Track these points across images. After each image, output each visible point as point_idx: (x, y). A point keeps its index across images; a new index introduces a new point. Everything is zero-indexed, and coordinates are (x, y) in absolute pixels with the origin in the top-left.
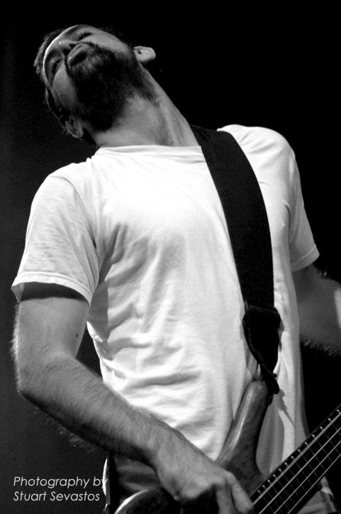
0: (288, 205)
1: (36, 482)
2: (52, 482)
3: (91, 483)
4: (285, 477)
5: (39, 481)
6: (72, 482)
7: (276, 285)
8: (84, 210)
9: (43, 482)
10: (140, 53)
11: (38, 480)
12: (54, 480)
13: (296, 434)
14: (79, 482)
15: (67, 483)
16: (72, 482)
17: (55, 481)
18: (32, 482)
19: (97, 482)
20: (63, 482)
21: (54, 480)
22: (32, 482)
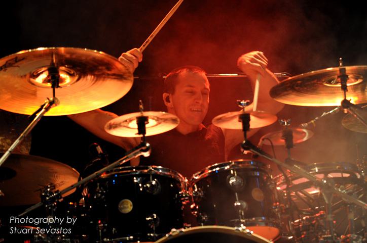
1: (26, 220)
2: (37, 221)
5: (28, 220)
6: (23, 221)
9: (31, 221)
11: (27, 218)
12: (39, 219)
14: (57, 220)
17: (40, 220)
18: (23, 221)
21: (39, 219)
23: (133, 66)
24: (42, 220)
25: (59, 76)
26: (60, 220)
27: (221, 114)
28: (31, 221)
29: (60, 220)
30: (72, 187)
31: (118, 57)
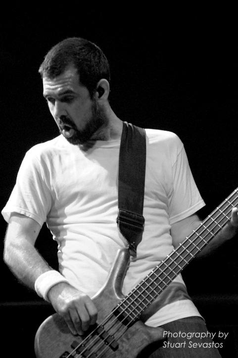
1: (178, 334)
2: (189, 335)
5: (181, 334)
6: (203, 335)
9: (175, 335)
11: (180, 333)
12: (191, 334)
14: (209, 335)
16: (203, 335)
17: (192, 334)
18: (175, 335)
21: (191, 334)
23: (72, 334)
24: (194, 334)
25: (198, 305)
26: (211, 335)
27: (41, 324)
28: (184, 335)
29: (211, 335)
30: (121, 252)
31: (185, 274)
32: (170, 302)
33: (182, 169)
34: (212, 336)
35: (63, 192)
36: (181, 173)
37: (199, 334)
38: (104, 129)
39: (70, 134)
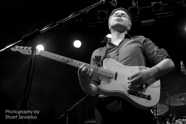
0: (97, 65)
1: (14, 112)
2: (19, 112)
3: (34, 112)
4: (133, 21)
5: (15, 112)
6: (26, 112)
7: (57, 55)
8: (158, 104)
9: (16, 112)
10: (101, 87)
11: (14, 111)
12: (24, 111)
13: (127, 41)
14: (29, 112)
15: (25, 112)
16: (26, 112)
17: (21, 112)
18: (12, 112)
19: (36, 112)
20: (23, 112)
21: (20, 111)
22: (12, 112)
24: (22, 112)
25: (130, 29)
26: (31, 112)
28: (16, 112)
29: (31, 112)
32: (161, 61)
33: (120, 79)
34: (31, 113)
35: (95, 112)
36: (120, 79)
37: (24, 111)
38: (92, 88)
39: (41, 52)
